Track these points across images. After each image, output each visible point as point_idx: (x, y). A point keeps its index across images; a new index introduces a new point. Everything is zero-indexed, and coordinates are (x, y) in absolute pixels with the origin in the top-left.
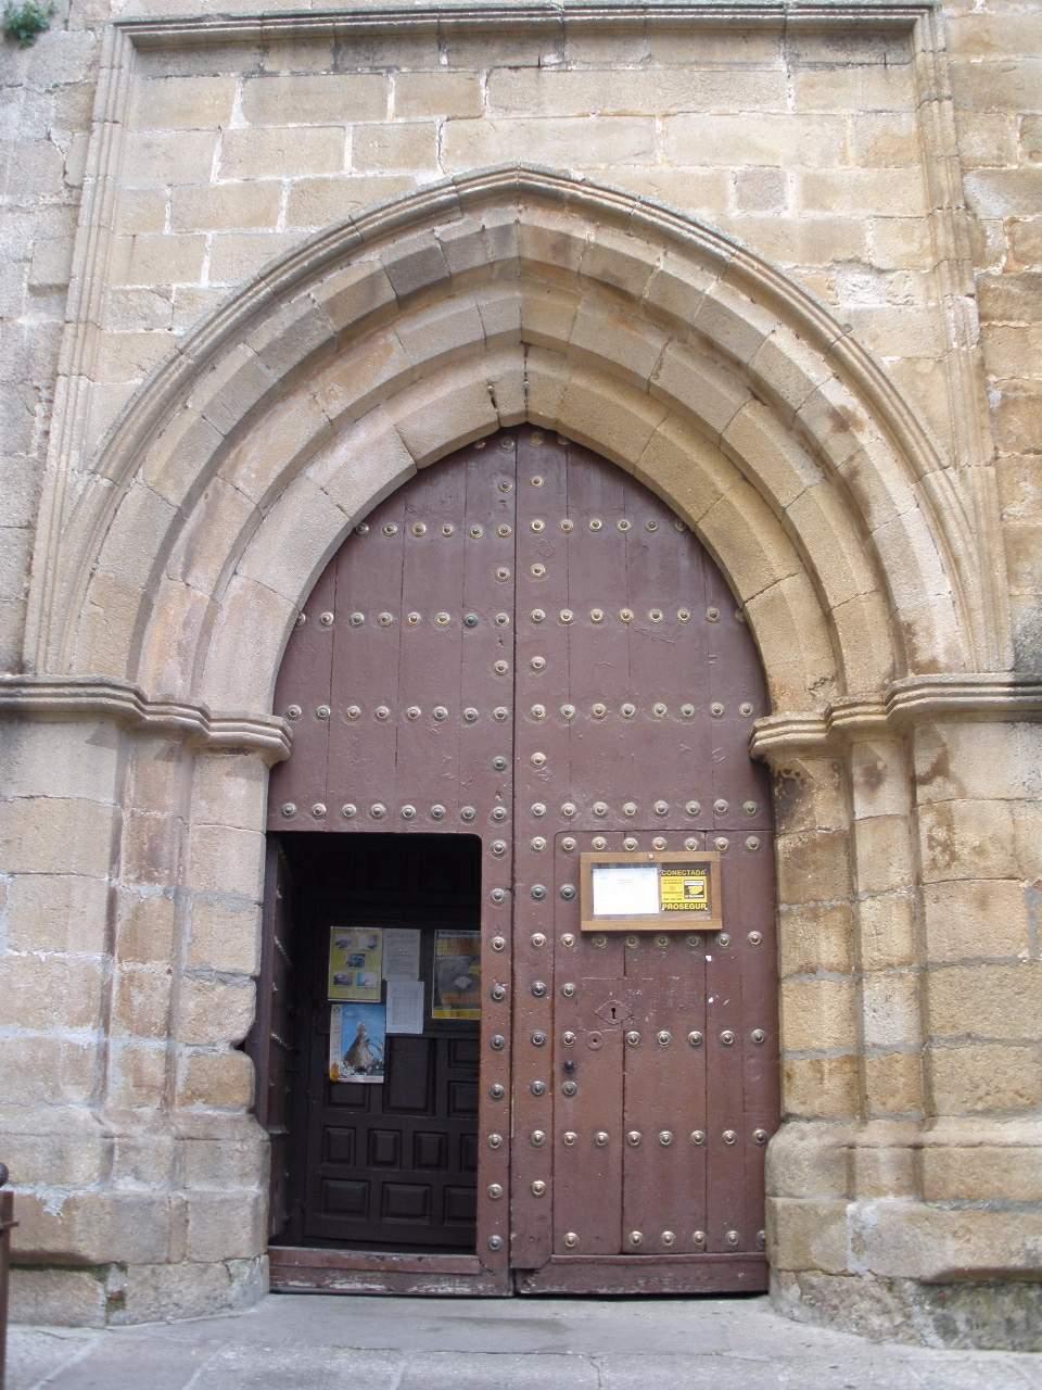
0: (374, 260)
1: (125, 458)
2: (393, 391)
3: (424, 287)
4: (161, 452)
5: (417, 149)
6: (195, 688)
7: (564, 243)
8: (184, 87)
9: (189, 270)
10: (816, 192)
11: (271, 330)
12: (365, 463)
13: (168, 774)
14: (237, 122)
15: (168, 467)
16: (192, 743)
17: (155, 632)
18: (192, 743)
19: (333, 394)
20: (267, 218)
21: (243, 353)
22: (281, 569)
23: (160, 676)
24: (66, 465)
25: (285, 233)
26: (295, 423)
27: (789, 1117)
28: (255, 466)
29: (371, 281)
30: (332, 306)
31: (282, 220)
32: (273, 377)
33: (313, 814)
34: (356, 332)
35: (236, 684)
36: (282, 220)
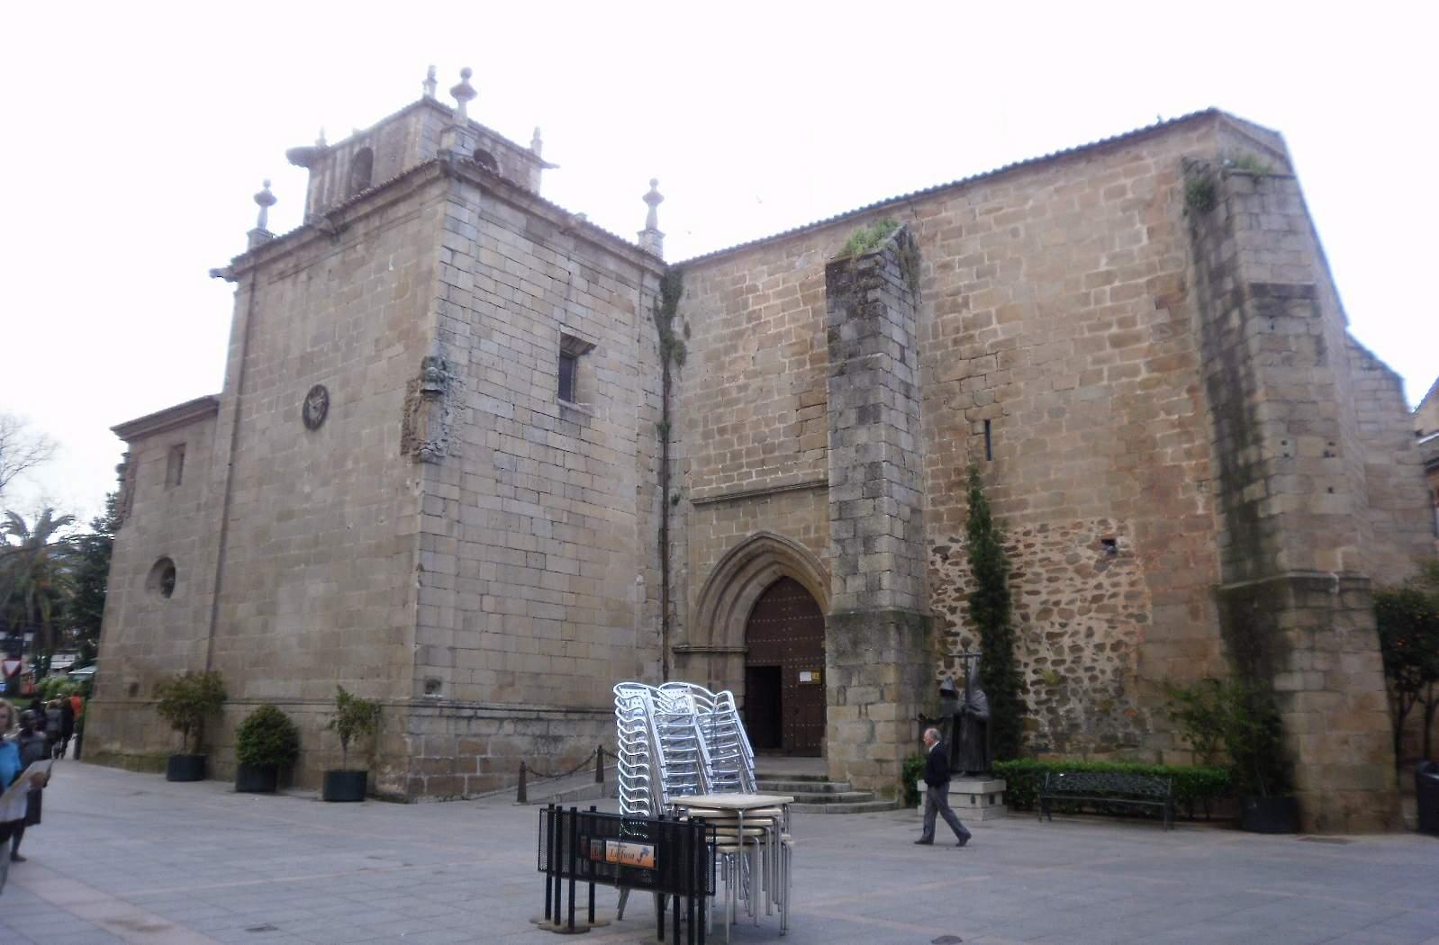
0: (740, 555)
1: (701, 601)
2: (755, 575)
3: (750, 559)
4: (708, 599)
5: (746, 527)
6: (725, 642)
7: (773, 547)
8: (704, 514)
9: (709, 559)
10: (817, 530)
11: (724, 572)
12: (753, 591)
13: (720, 661)
14: (715, 522)
15: (710, 604)
16: (724, 654)
17: (714, 633)
18: (724, 654)
19: (741, 580)
20: (721, 546)
21: (720, 577)
22: (740, 616)
23: (717, 642)
24: (692, 604)
25: (725, 549)
26: (735, 587)
27: (1272, 476)
28: (728, 599)
29: (740, 560)
30: (734, 565)
31: (1064, 430)
32: (727, 580)
33: (754, 662)
34: (742, 568)
35: (735, 640)
36: (1064, 430)
